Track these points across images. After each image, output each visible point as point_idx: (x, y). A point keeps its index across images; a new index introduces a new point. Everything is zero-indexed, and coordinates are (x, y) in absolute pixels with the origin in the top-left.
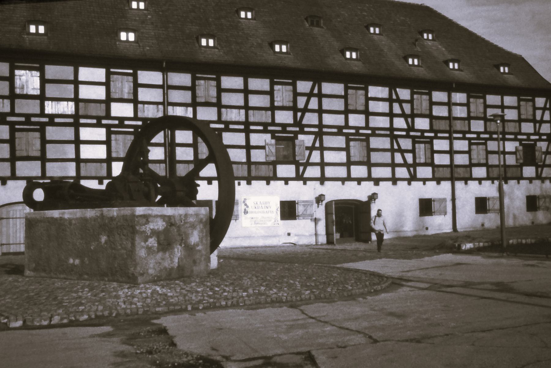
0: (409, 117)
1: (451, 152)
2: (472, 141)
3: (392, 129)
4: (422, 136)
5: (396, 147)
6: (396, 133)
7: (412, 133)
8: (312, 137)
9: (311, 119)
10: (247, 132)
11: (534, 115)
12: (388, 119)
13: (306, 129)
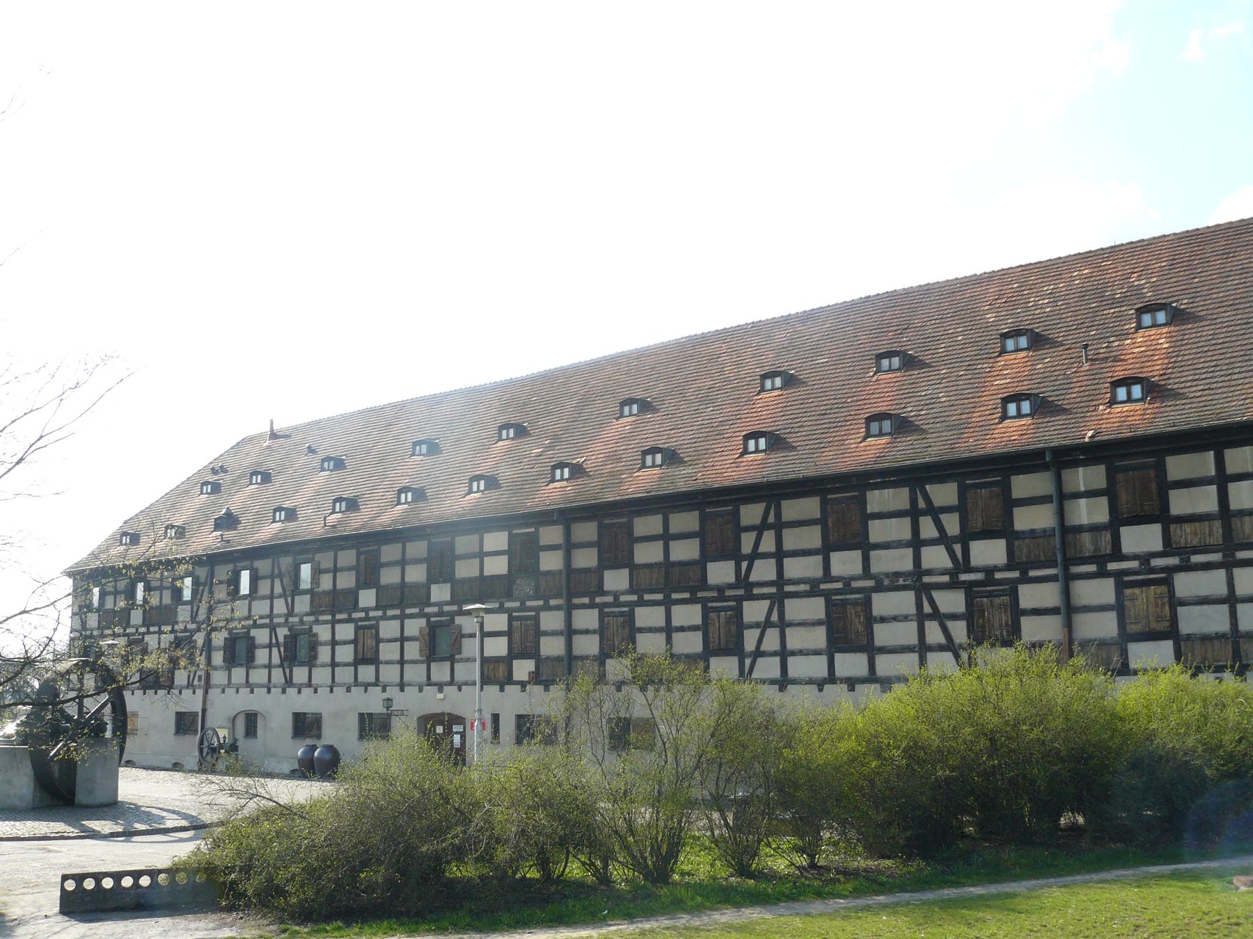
0: (922, 509)
1: (669, 630)
2: (607, 610)
3: (919, 571)
4: (617, 603)
5: (927, 609)
6: (926, 579)
7: (964, 577)
8: (766, 604)
9: (764, 571)
10: (780, 581)
11: (296, 615)
12: (907, 521)
13: (756, 591)
